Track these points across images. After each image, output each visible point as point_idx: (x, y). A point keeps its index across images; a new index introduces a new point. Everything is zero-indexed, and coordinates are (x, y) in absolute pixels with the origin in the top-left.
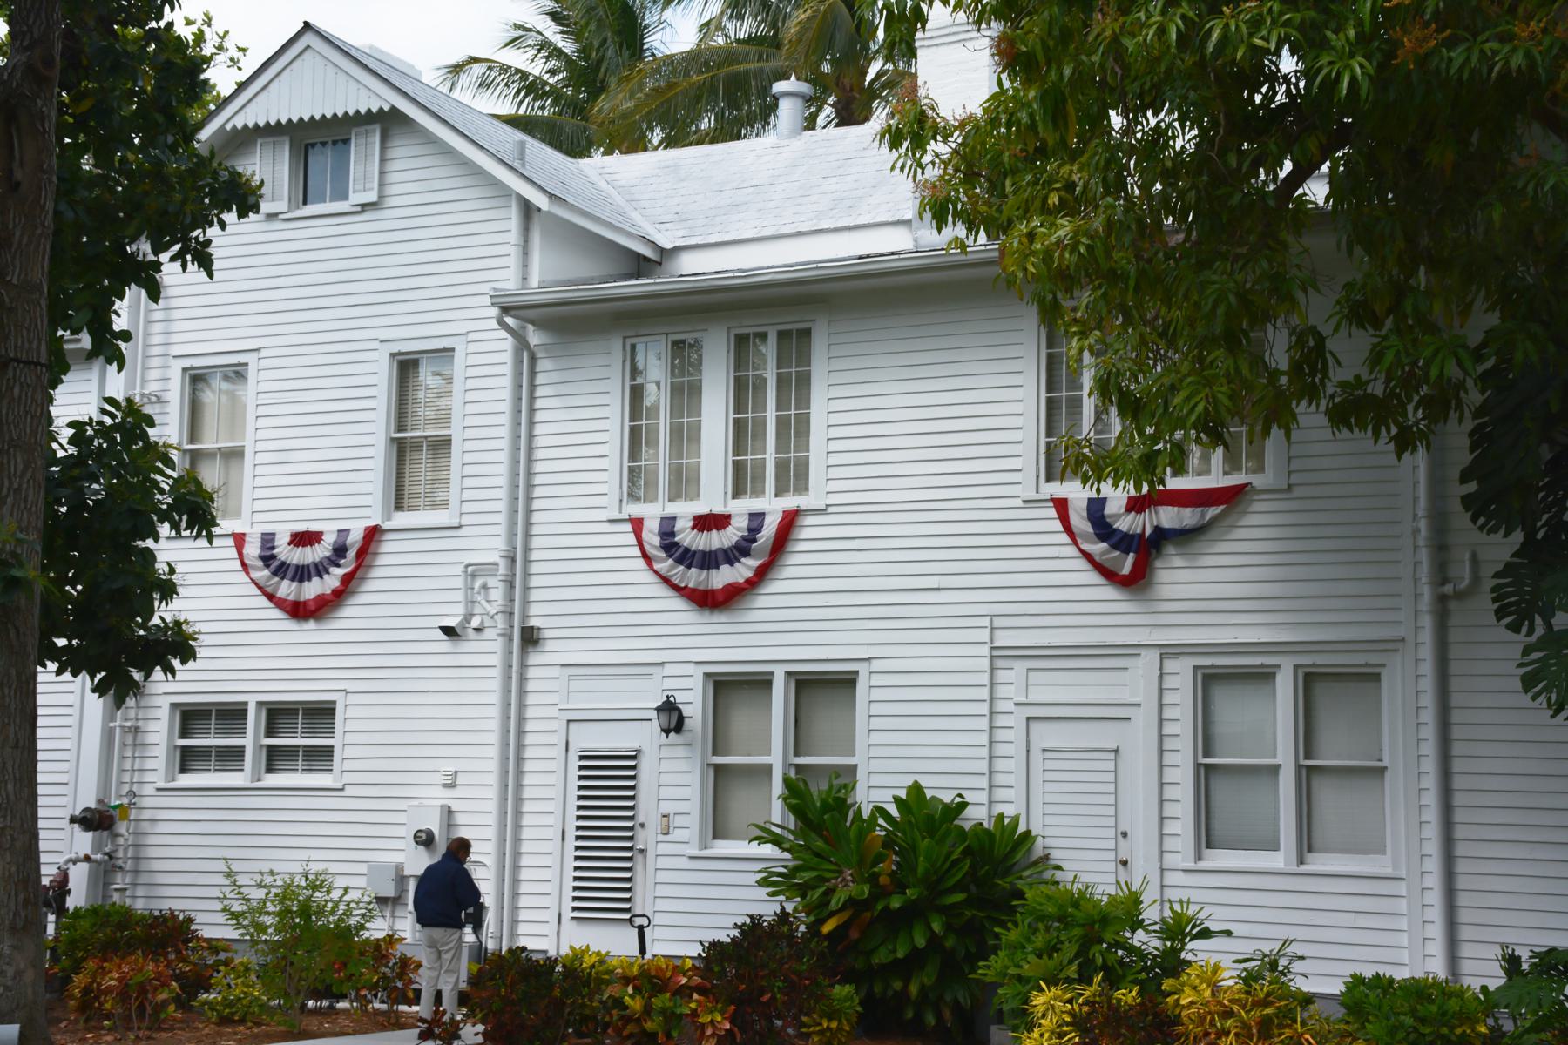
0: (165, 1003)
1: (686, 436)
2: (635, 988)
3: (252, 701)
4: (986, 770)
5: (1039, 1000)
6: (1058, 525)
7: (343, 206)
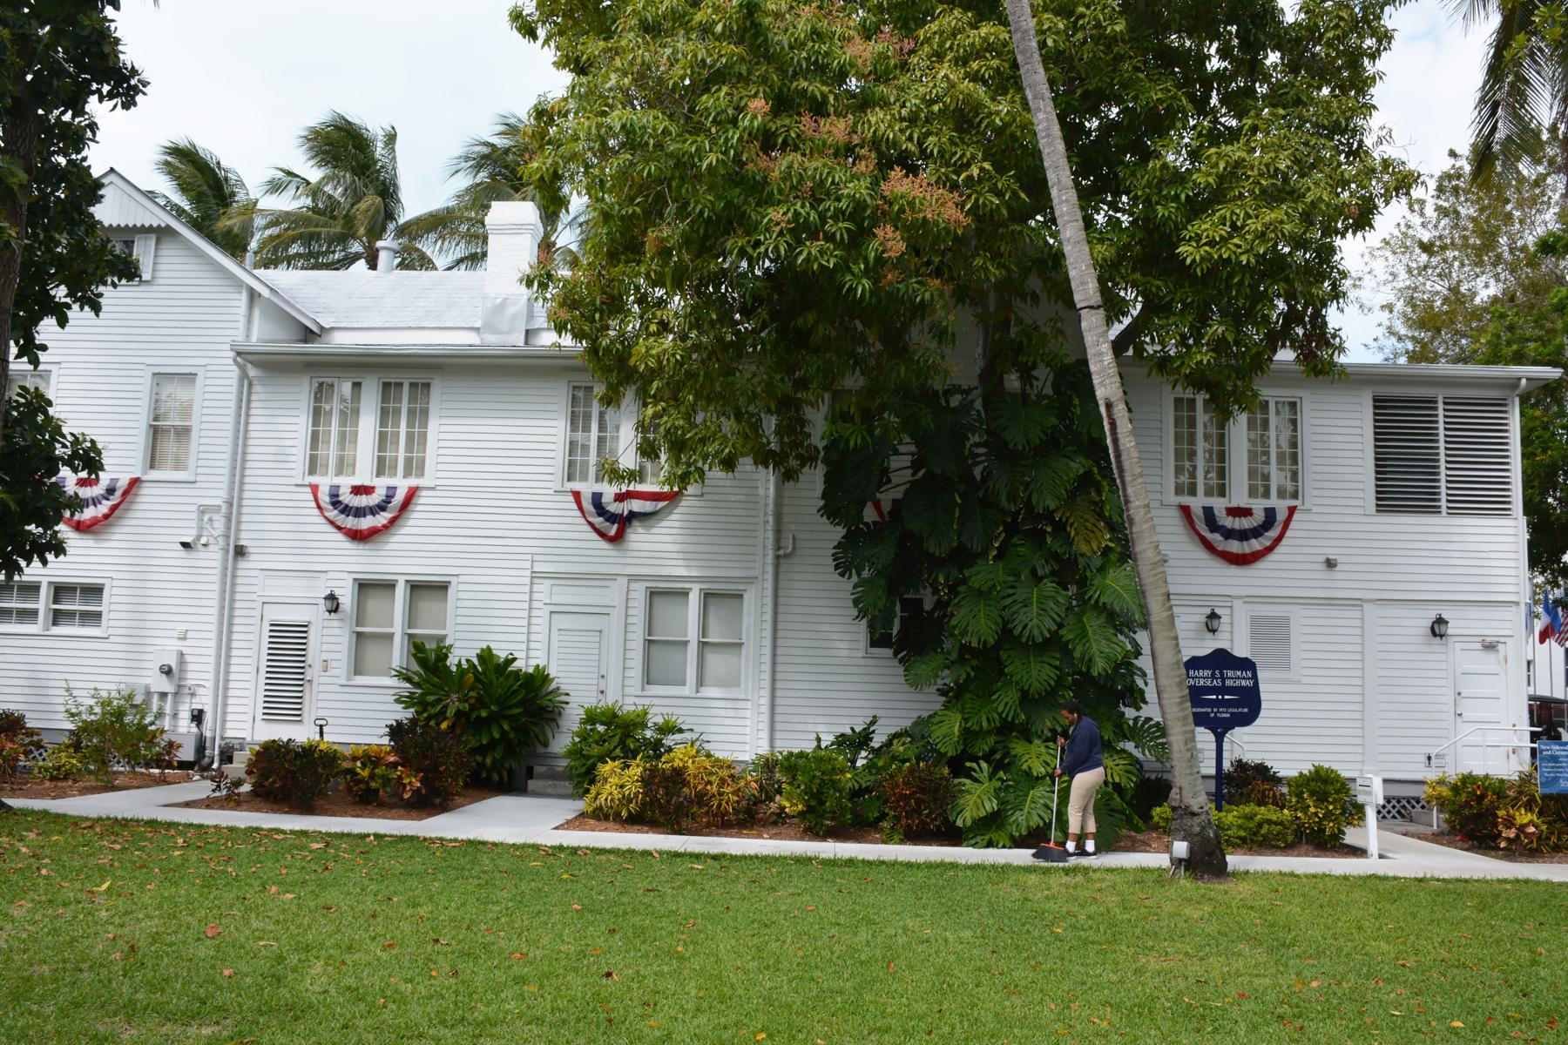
3: (44, 582)
6: (575, 506)
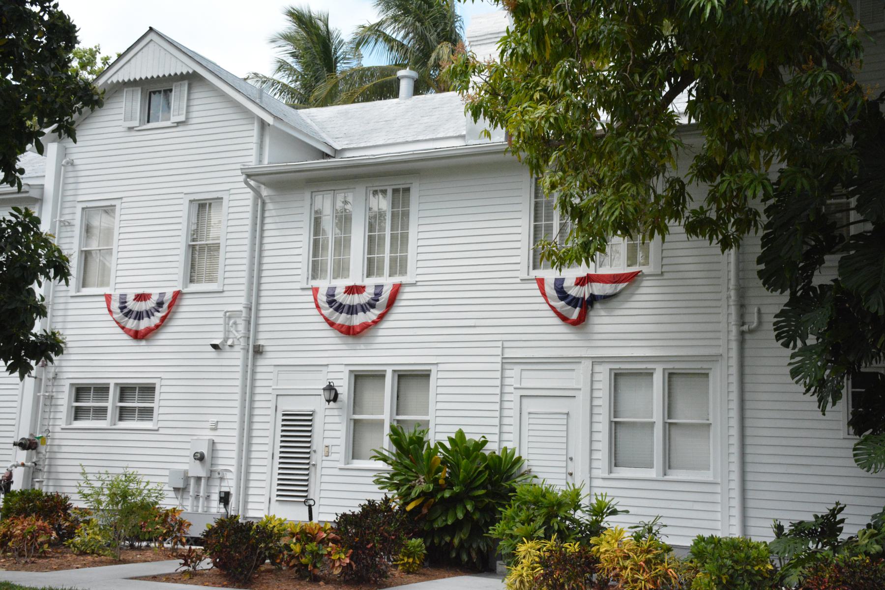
0: (42, 544)
1: (343, 244)
2: (297, 539)
3: (112, 383)
4: (498, 424)
5: (522, 549)
6: (539, 293)
7: (168, 124)
